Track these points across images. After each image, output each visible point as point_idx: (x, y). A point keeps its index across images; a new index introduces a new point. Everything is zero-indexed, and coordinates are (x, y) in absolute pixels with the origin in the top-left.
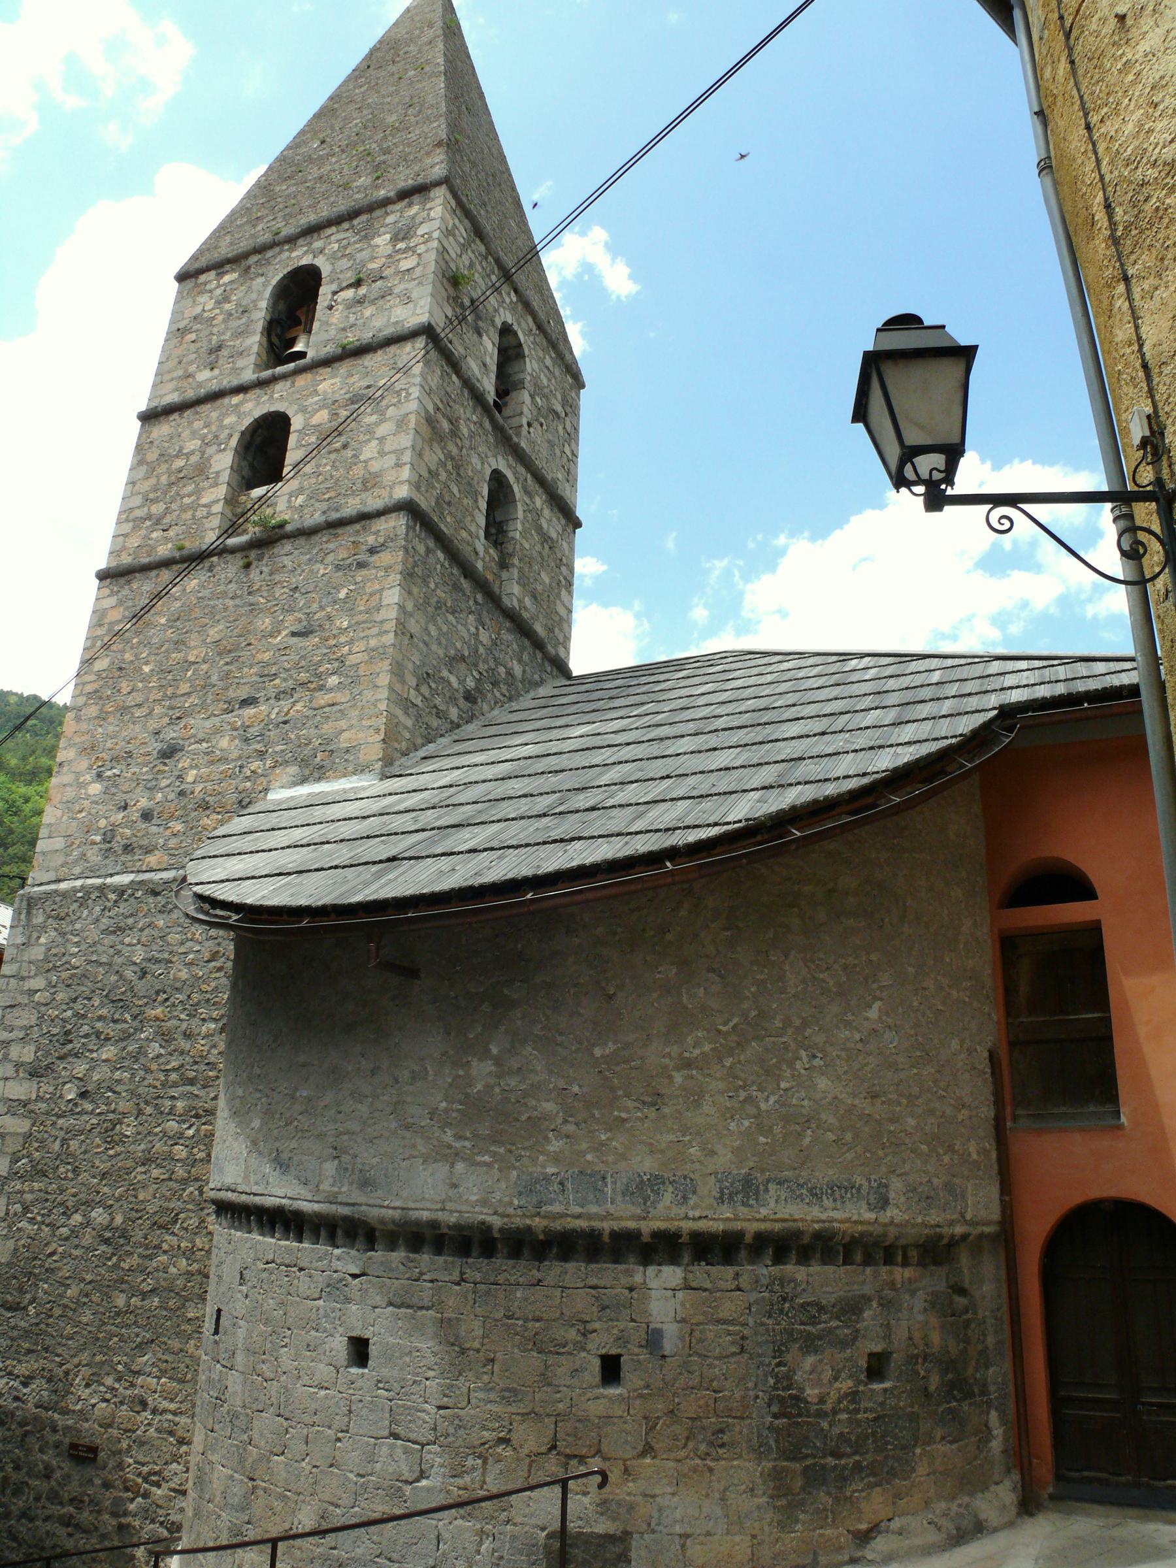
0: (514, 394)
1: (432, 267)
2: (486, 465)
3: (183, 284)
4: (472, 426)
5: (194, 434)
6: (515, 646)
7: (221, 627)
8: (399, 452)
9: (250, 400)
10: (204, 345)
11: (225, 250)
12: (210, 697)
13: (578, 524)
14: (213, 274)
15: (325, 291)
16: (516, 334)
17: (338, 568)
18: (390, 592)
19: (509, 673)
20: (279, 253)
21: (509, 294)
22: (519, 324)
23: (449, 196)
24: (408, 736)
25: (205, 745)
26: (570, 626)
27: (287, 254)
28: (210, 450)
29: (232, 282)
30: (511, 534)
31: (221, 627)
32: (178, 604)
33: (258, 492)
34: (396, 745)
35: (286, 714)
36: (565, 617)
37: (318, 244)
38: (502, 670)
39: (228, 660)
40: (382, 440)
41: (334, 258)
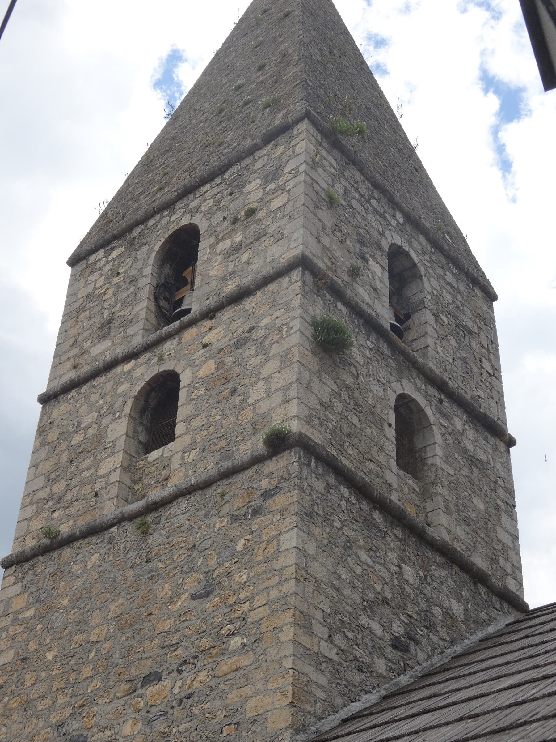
0: (415, 316)
1: (302, 199)
2: (389, 391)
3: (76, 267)
4: (367, 352)
5: (91, 407)
6: (450, 582)
7: (121, 601)
8: (286, 388)
9: (141, 365)
10: (97, 320)
11: (114, 229)
12: (112, 677)
13: (511, 442)
14: (101, 253)
15: (204, 245)
16: (407, 255)
17: (235, 518)
18: (287, 536)
19: (447, 613)
20: (161, 219)
21: (394, 216)
22: (410, 245)
23: (312, 130)
24: (322, 695)
25: (108, 733)
26: (518, 554)
27: (166, 219)
28: (105, 421)
29: (119, 256)
30: (430, 461)
31: (121, 601)
32: (79, 582)
33: (154, 455)
34: (309, 708)
35: (189, 687)
36: (510, 544)
37: (194, 204)
38: (437, 611)
39: (128, 635)
40: (268, 379)
41: (209, 214)
